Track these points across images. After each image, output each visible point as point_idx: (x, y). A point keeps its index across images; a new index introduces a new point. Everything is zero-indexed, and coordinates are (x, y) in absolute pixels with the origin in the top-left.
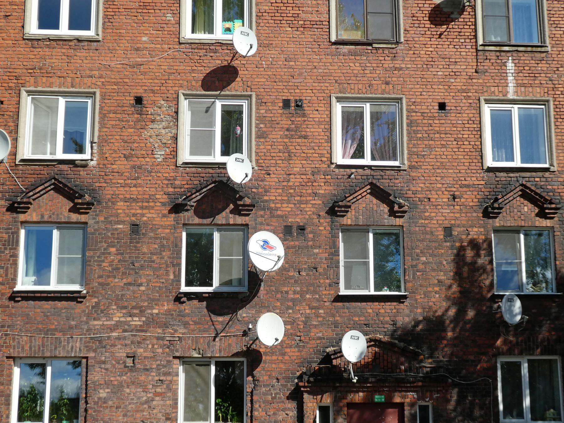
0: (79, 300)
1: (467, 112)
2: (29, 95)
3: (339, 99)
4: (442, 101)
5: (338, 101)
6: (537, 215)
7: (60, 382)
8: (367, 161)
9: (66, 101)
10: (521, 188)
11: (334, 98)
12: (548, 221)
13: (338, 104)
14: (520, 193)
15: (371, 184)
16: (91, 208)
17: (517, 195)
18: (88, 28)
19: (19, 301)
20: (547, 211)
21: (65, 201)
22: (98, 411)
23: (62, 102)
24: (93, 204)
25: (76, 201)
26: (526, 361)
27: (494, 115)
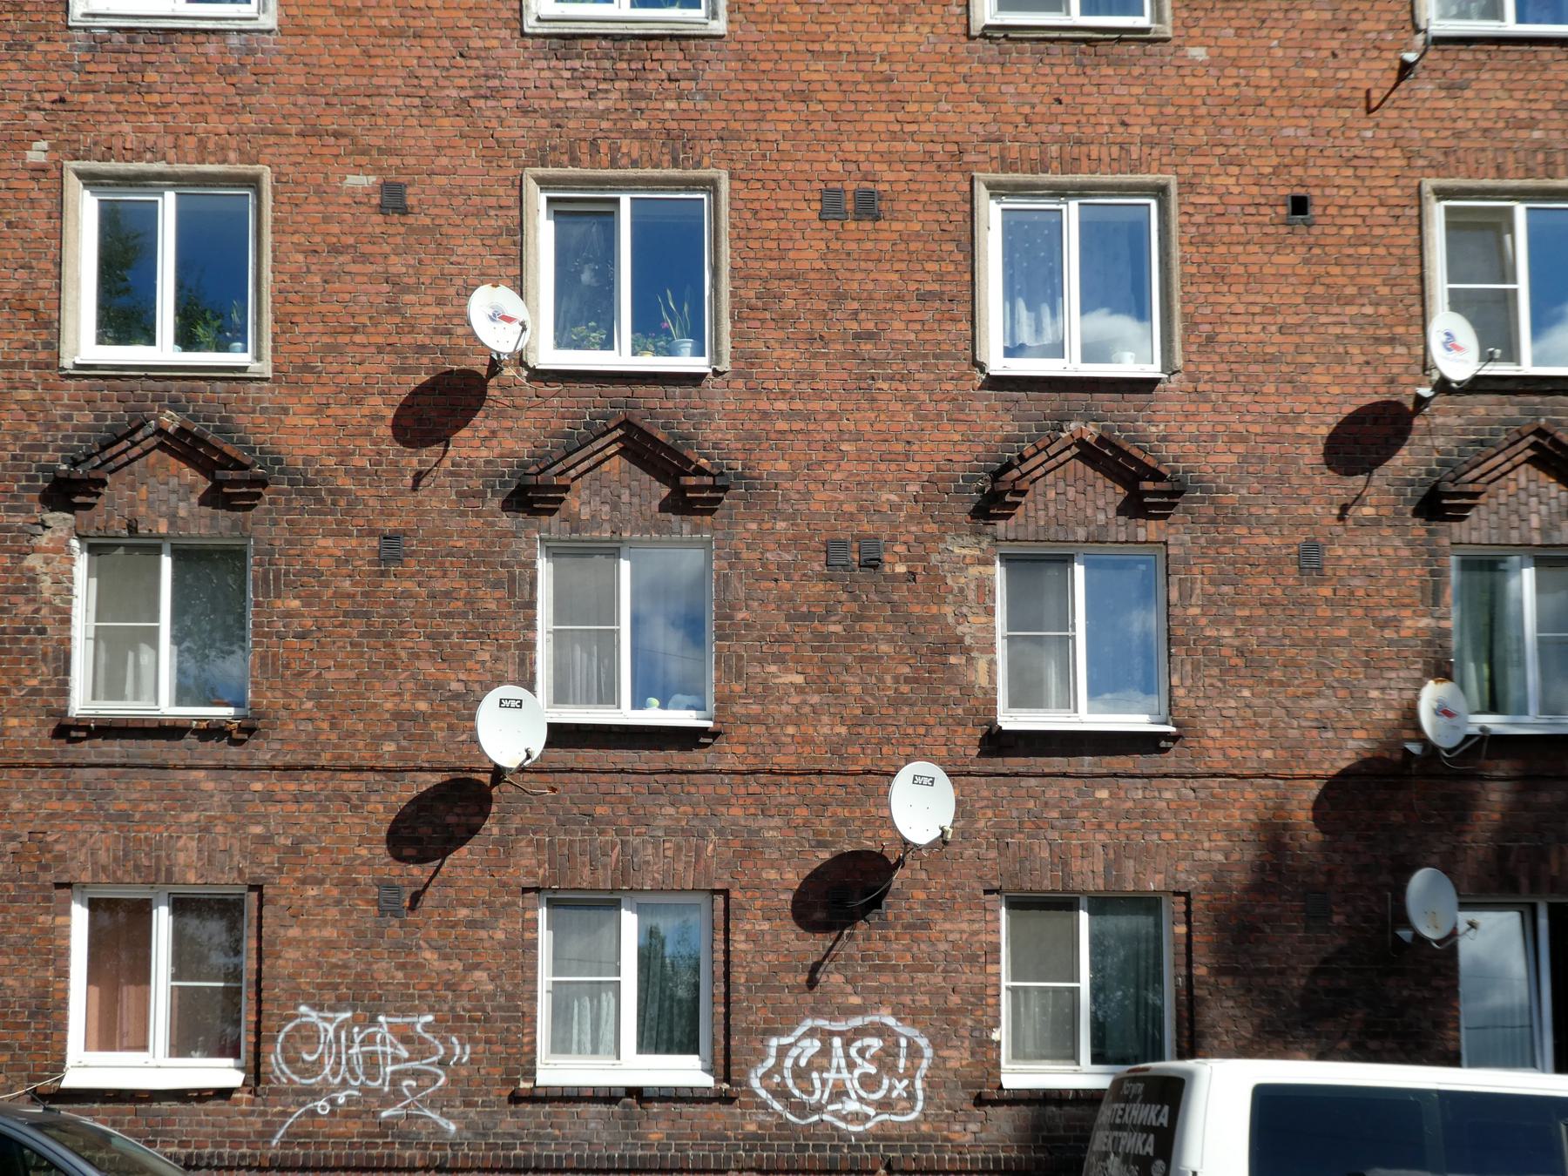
0: (73, 734)
1: (921, 216)
2: (1439, 200)
3: (997, 190)
4: (1300, 191)
5: (992, 195)
6: (1121, 511)
7: (1034, 995)
8: (164, 351)
9: (1004, 210)
10: (1532, 439)
11: (983, 188)
12: (1152, 524)
13: (993, 202)
14: (1530, 453)
15: (626, 424)
16: (259, 496)
17: (1521, 457)
18: (1141, 14)
19: (79, 740)
20: (1147, 500)
21: (189, 474)
22: (422, 1041)
23: (1072, 211)
24: (103, 483)
25: (220, 474)
26: (164, 896)
27: (1013, 228)
